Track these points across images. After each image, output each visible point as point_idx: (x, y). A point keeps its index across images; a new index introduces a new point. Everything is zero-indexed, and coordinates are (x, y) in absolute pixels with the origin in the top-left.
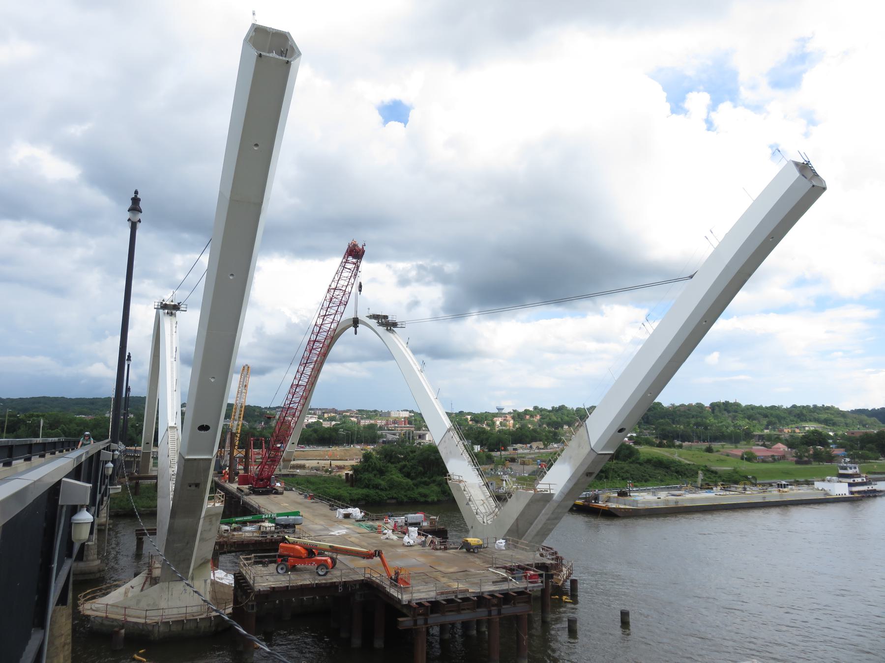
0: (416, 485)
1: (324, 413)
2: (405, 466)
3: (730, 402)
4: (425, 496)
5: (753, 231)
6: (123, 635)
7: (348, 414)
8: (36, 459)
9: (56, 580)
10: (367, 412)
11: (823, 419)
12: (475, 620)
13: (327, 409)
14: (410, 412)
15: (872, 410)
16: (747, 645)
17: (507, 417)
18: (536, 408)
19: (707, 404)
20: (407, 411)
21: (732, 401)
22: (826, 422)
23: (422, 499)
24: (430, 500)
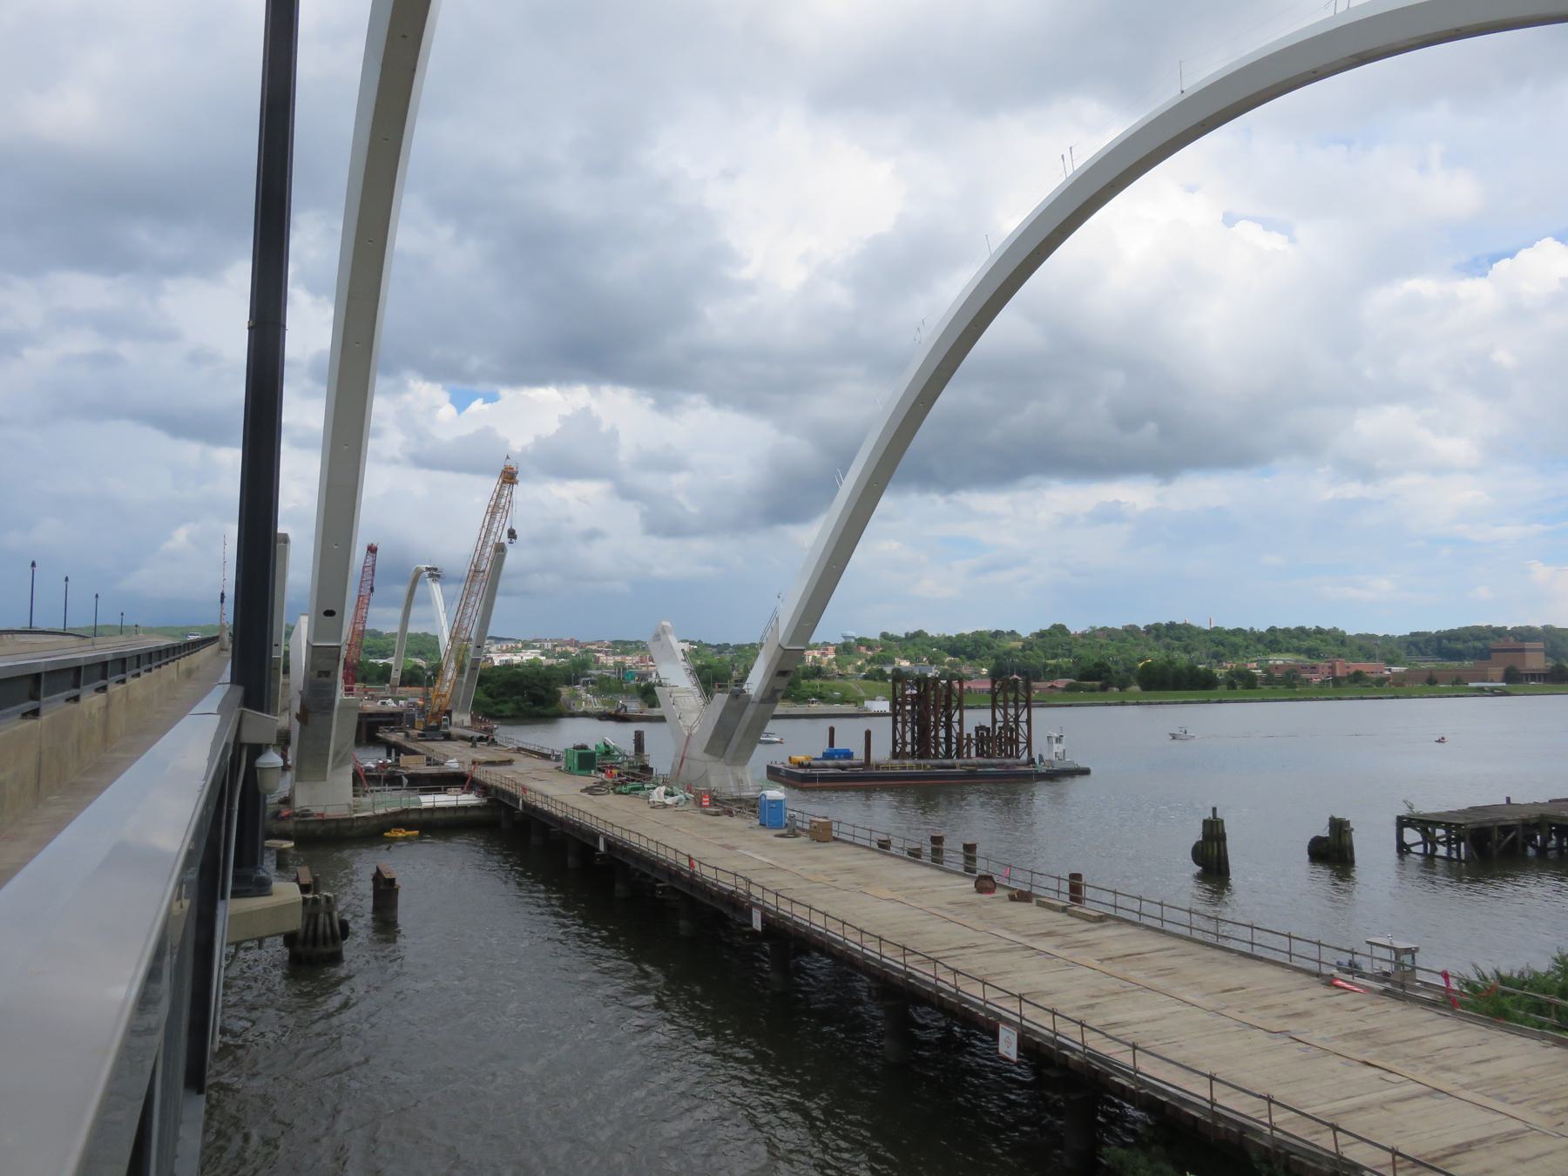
0: (496, 704)
1: (555, 646)
2: (488, 688)
3: (1177, 623)
4: (501, 711)
5: (943, 334)
6: (1219, 1126)
7: (594, 647)
8: (768, 835)
9: (224, 782)
10: (625, 643)
11: (1304, 647)
12: (81, 687)
13: (561, 639)
14: (692, 643)
15: (1437, 632)
16: (1341, 905)
17: (827, 650)
18: (884, 636)
19: (1340, 630)
20: (686, 641)
21: (1179, 621)
22: (1311, 652)
23: (499, 714)
24: (504, 714)
